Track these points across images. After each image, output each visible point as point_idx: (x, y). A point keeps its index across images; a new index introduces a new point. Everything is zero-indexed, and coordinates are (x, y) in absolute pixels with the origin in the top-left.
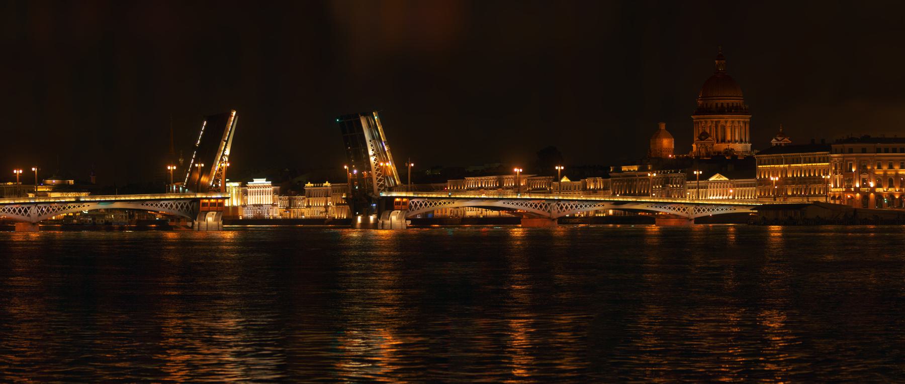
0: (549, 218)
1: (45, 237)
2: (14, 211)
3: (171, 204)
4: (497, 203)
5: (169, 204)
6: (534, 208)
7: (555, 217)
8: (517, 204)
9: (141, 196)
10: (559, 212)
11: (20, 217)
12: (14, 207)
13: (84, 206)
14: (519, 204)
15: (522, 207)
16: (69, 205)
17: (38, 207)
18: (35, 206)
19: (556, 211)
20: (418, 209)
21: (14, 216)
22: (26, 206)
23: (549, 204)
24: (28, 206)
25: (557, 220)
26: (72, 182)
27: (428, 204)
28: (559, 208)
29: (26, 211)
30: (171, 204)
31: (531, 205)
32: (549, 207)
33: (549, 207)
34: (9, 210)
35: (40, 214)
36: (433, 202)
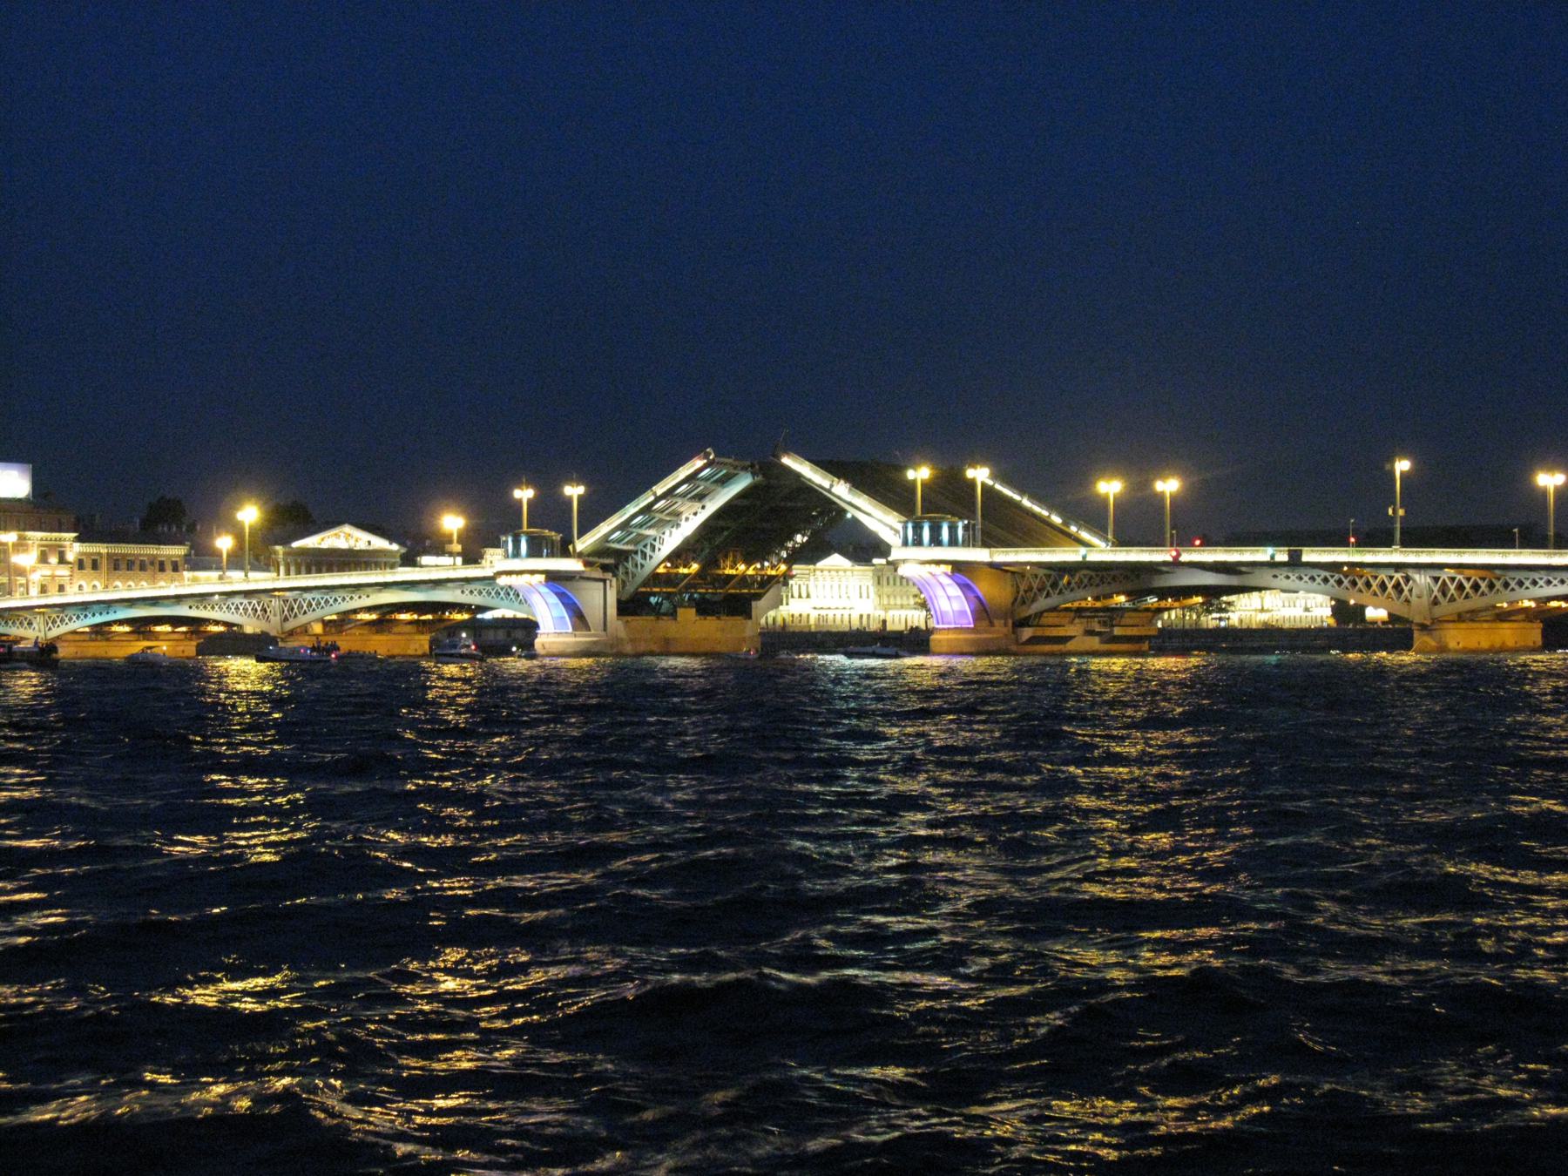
10: (1435, 602)
29: (1397, 586)
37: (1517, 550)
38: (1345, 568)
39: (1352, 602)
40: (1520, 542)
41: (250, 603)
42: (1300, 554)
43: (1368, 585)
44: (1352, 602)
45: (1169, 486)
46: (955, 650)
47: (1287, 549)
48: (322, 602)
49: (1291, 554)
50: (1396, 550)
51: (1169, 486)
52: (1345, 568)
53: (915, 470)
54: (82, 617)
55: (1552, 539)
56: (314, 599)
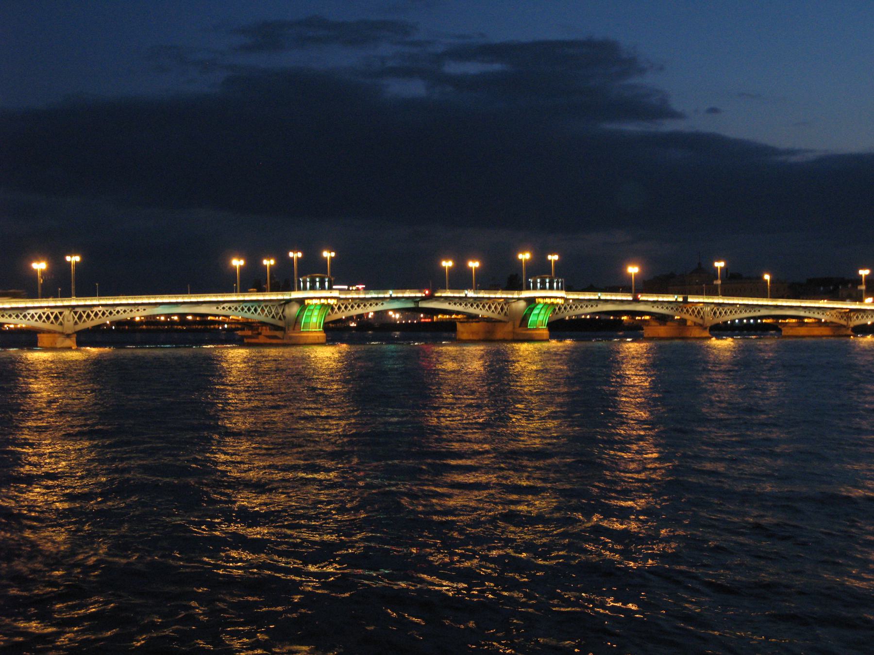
0: (62, 333)
1: (455, 507)
2: (48, 317)
3: (249, 307)
4: (156, 309)
5: (107, 311)
6: (690, 314)
7: (69, 332)
8: (230, 308)
9: (380, 293)
10: (76, 323)
11: (47, 326)
12: (40, 311)
13: (138, 310)
14: (233, 309)
15: (16, 320)
16: (119, 308)
17: (74, 312)
18: (71, 311)
19: (72, 322)
20: (92, 319)
21: (39, 324)
22: (56, 311)
23: (61, 313)
24: (60, 310)
25: (75, 335)
26: (235, 285)
27: (343, 308)
28: (76, 317)
29: (56, 318)
30: (249, 307)
31: (33, 317)
32: (702, 313)
33: (702, 313)
34: (33, 317)
35: (76, 322)
36: (246, 307)
37: (60, 299)
38: (738, 306)
39: (344, 317)
40: (771, 294)
41: (723, 310)
42: (687, 298)
43: (687, 311)
44: (344, 317)
45: (474, 264)
46: (502, 324)
47: (682, 296)
48: (85, 316)
49: (683, 298)
50: (74, 299)
51: (474, 264)
52: (738, 306)
53: (71, 257)
54: (748, 311)
55: (39, 291)
56: (44, 313)
